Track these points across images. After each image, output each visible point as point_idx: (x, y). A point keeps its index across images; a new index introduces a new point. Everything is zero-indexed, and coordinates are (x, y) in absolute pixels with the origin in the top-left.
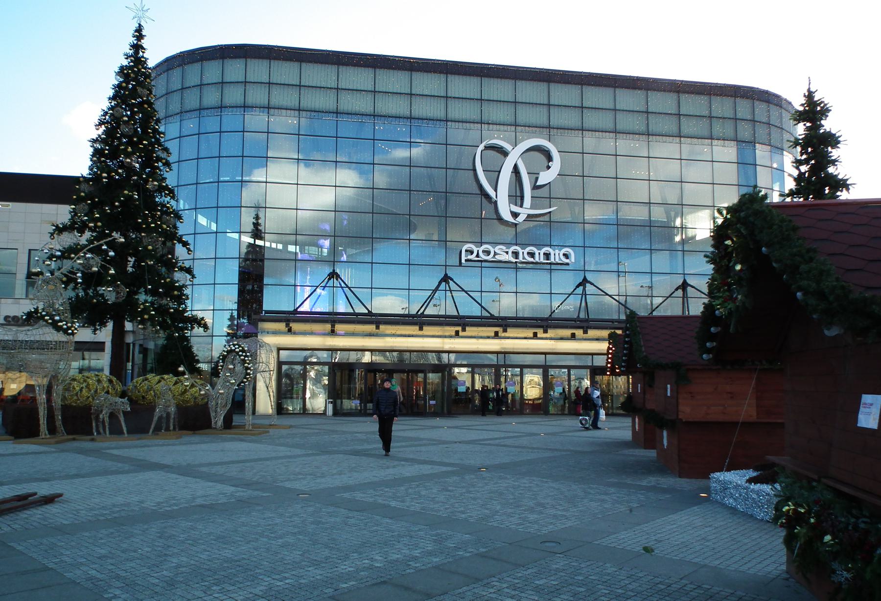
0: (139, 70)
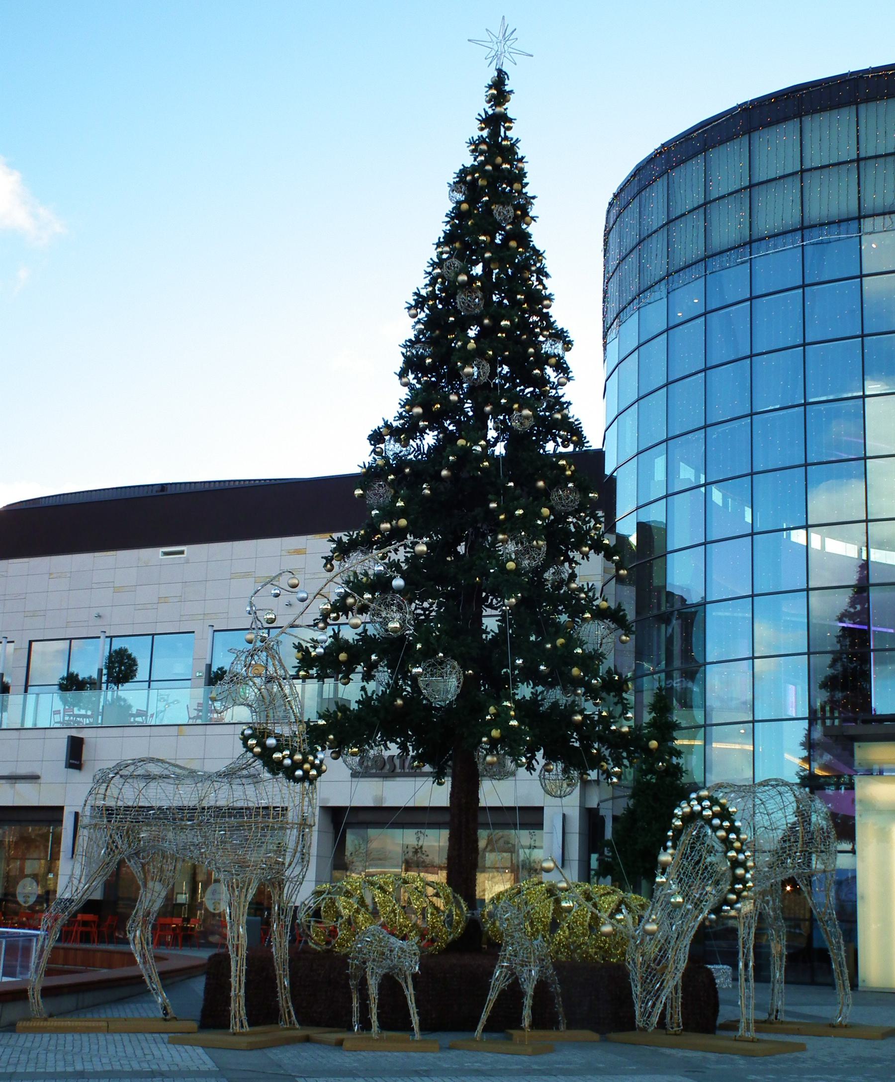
0: (497, 167)
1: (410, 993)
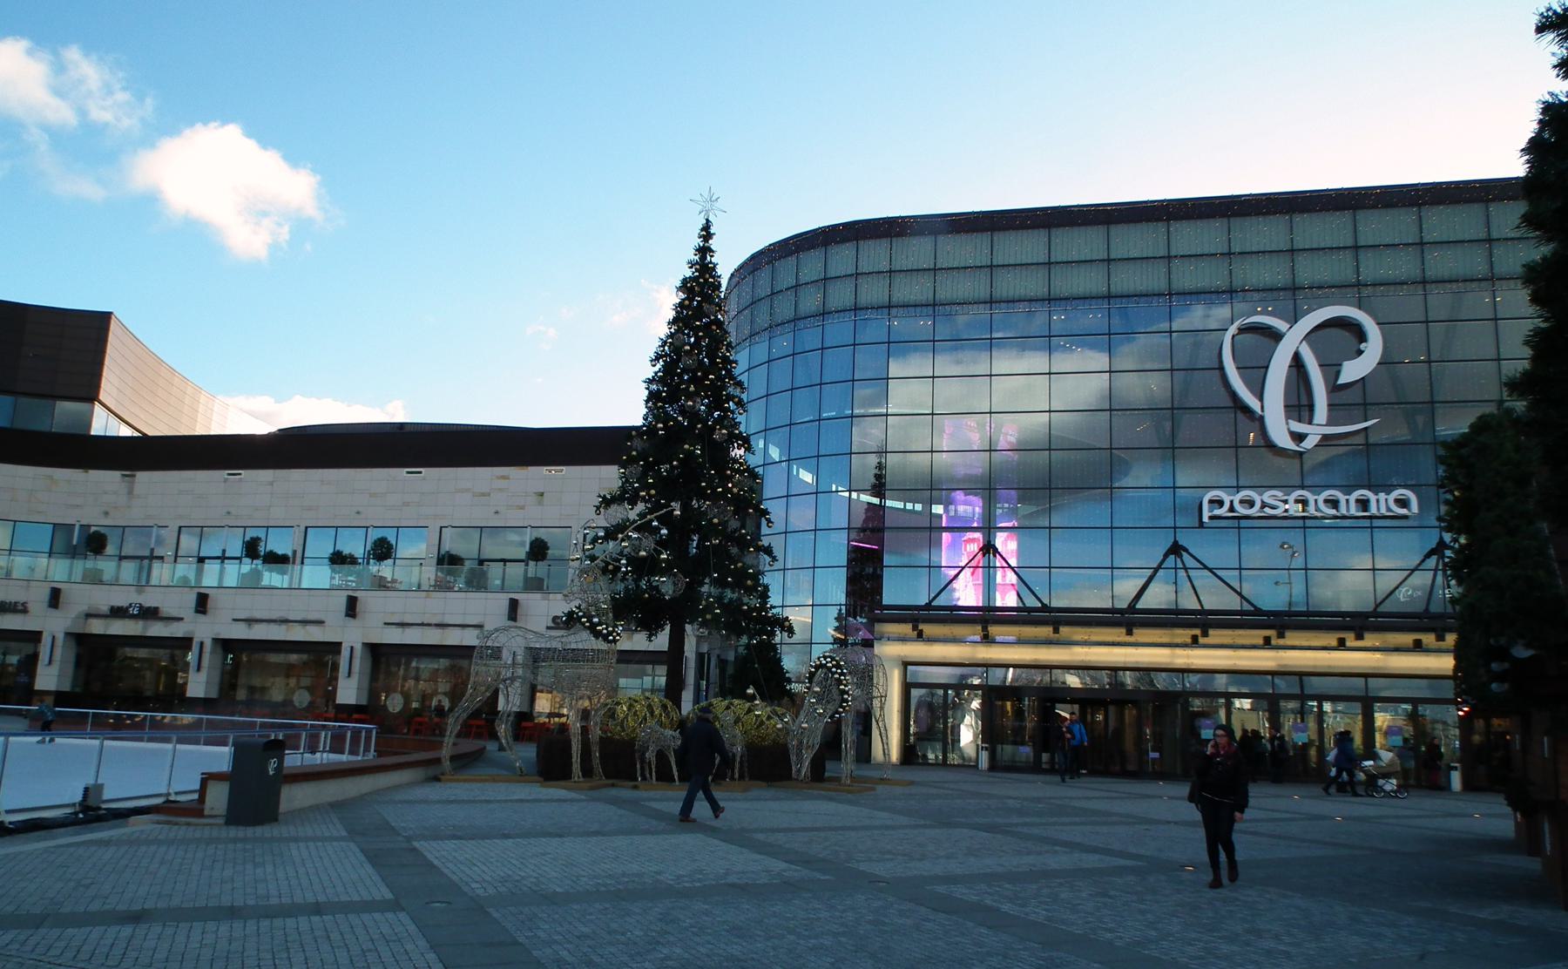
0: (706, 280)
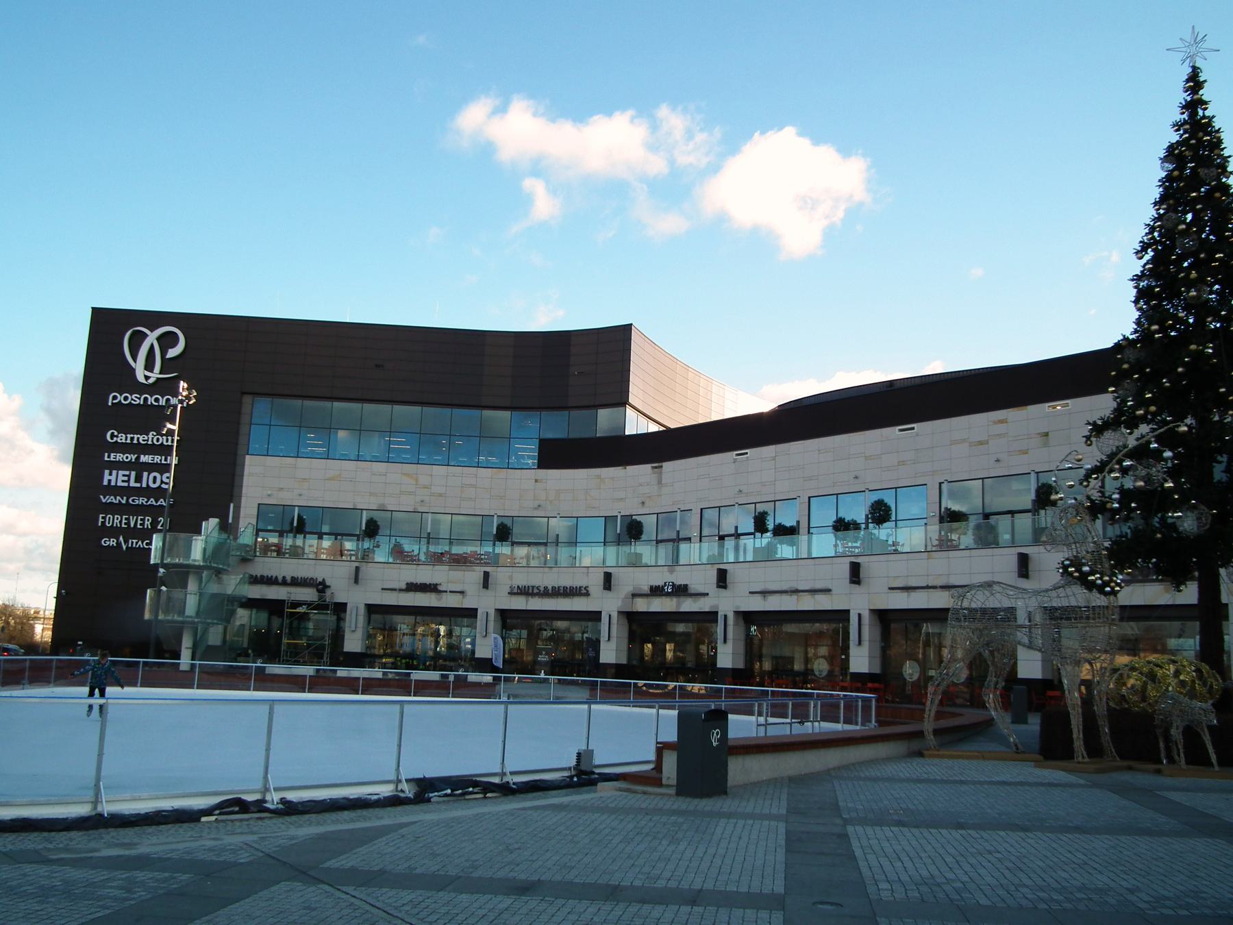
0: (1200, 141)
1: (1207, 739)
